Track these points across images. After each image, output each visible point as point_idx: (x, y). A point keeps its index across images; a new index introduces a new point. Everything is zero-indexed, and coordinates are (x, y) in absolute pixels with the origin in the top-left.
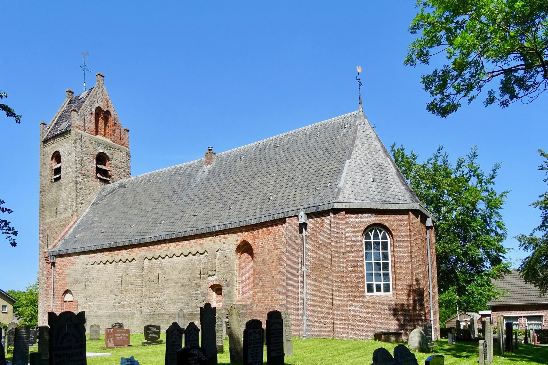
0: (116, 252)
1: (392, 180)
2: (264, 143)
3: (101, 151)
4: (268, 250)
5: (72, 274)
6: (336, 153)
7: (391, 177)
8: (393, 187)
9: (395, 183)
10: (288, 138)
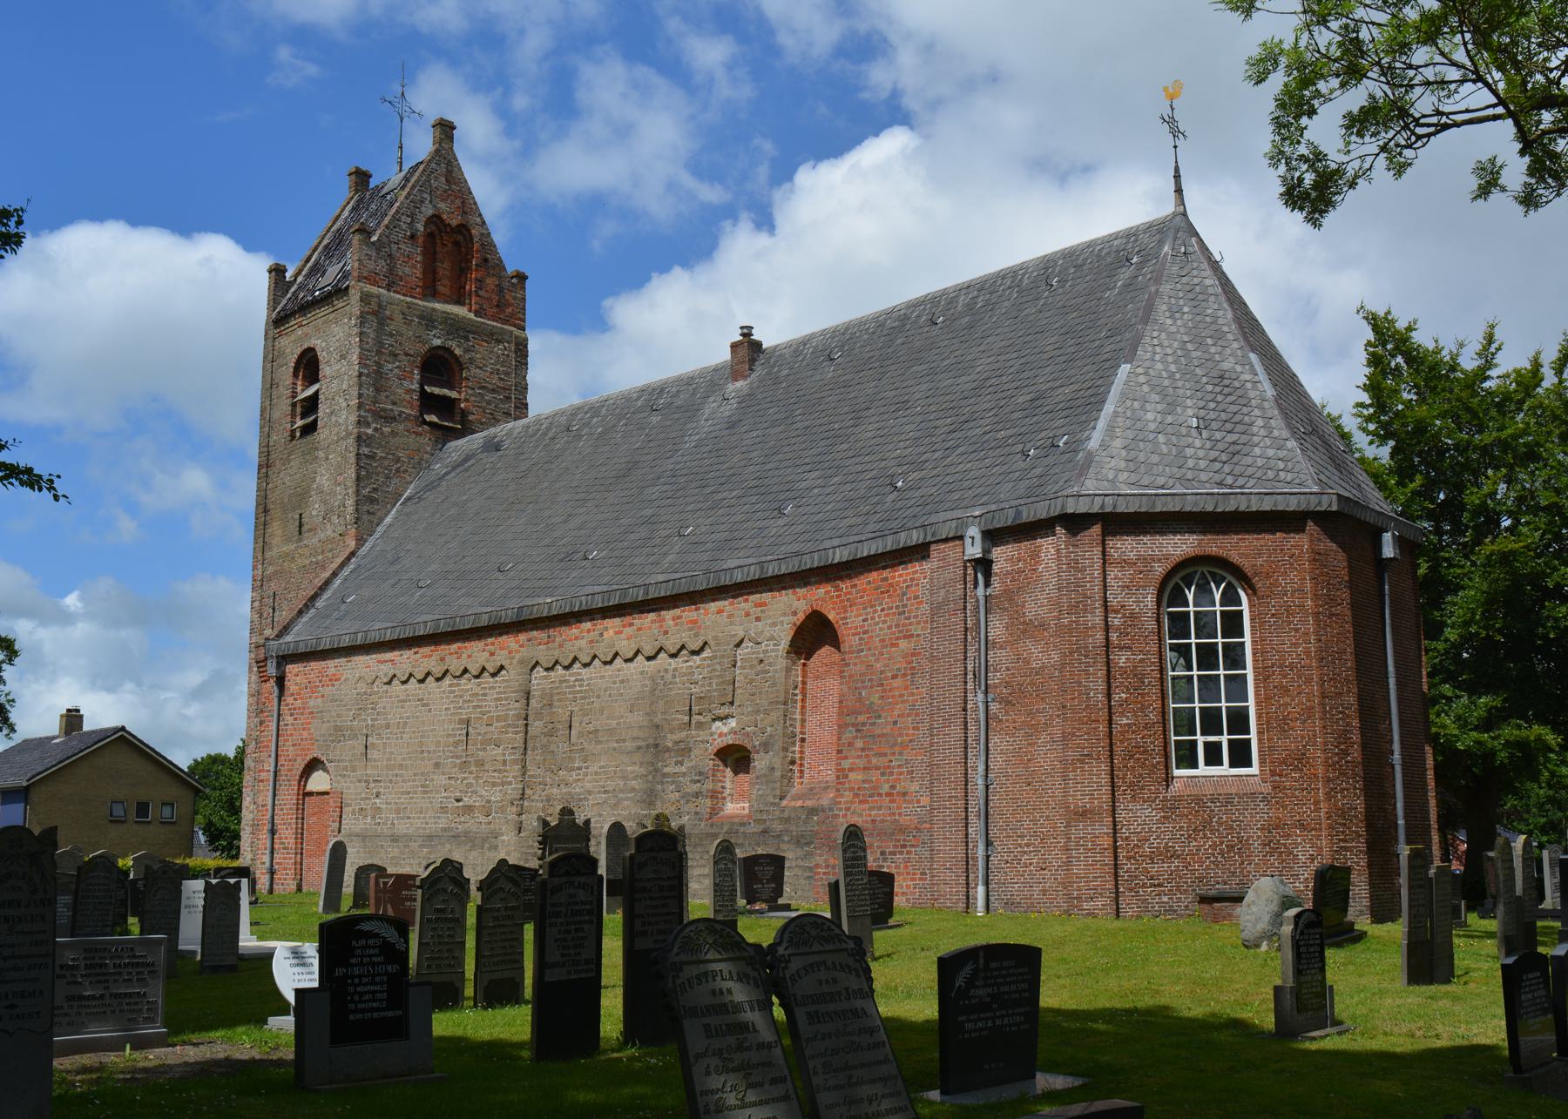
0: (454, 647)
1: (1260, 422)
2: (902, 312)
3: (437, 342)
4: (882, 641)
5: (330, 711)
6: (1097, 343)
7: (1257, 412)
8: (1261, 445)
9: (1270, 429)
10: (970, 296)
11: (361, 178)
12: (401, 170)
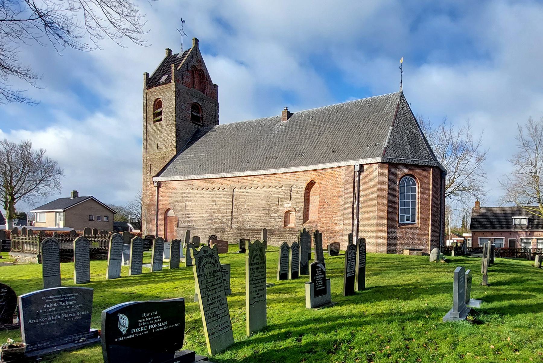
3: (195, 101)
11: (169, 51)
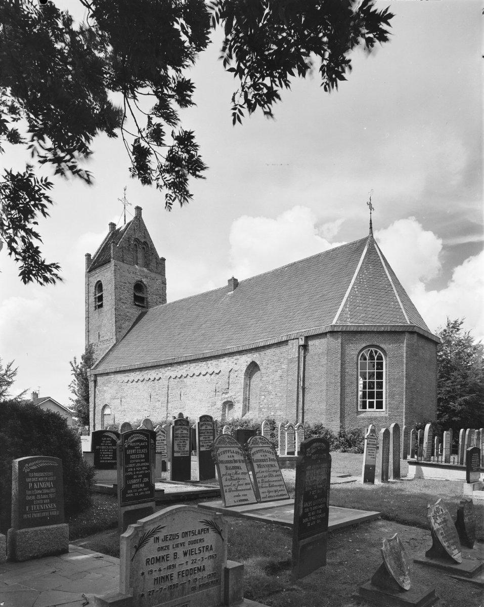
12: (125, 223)
